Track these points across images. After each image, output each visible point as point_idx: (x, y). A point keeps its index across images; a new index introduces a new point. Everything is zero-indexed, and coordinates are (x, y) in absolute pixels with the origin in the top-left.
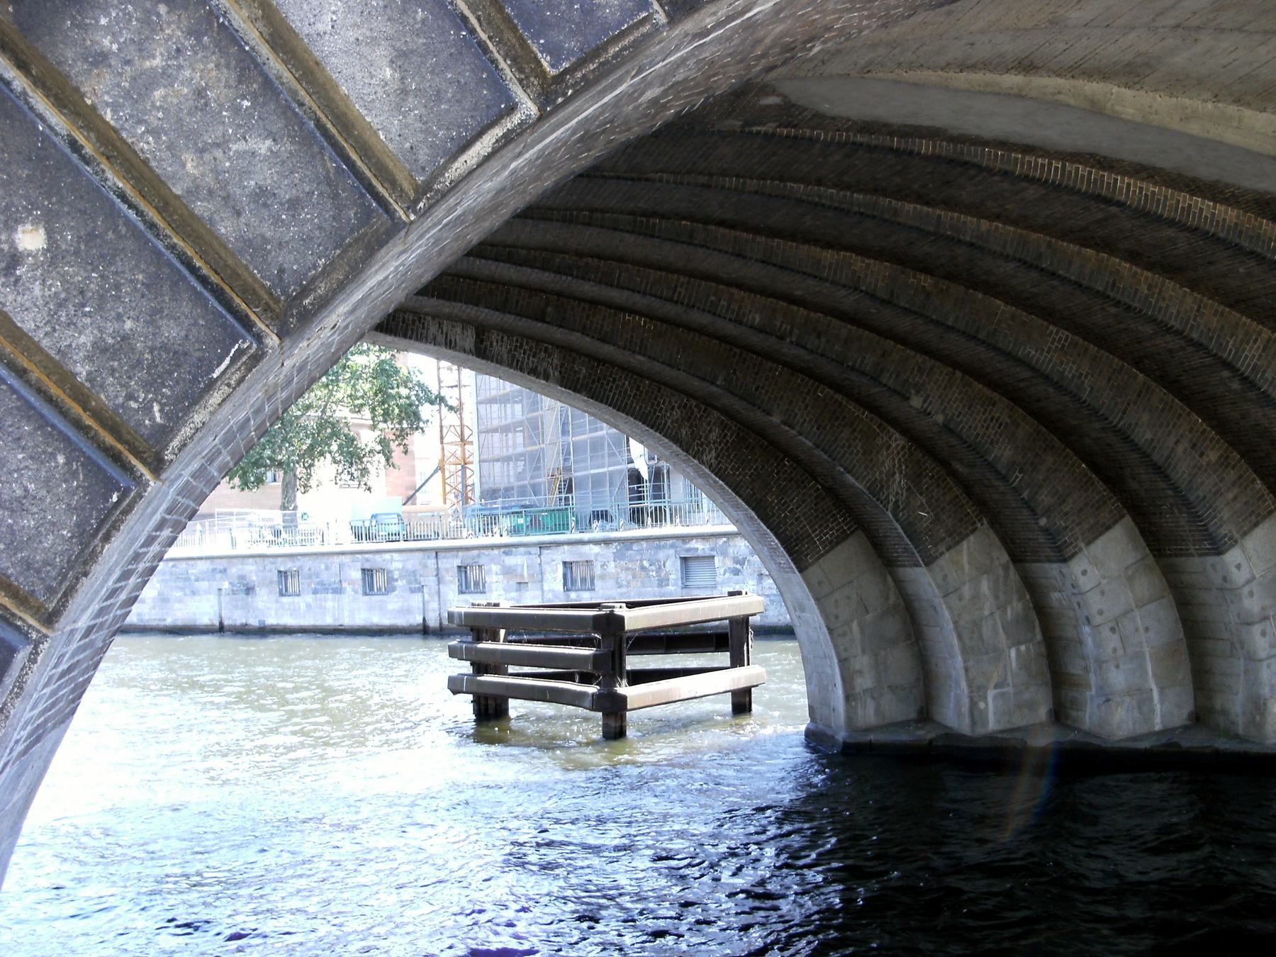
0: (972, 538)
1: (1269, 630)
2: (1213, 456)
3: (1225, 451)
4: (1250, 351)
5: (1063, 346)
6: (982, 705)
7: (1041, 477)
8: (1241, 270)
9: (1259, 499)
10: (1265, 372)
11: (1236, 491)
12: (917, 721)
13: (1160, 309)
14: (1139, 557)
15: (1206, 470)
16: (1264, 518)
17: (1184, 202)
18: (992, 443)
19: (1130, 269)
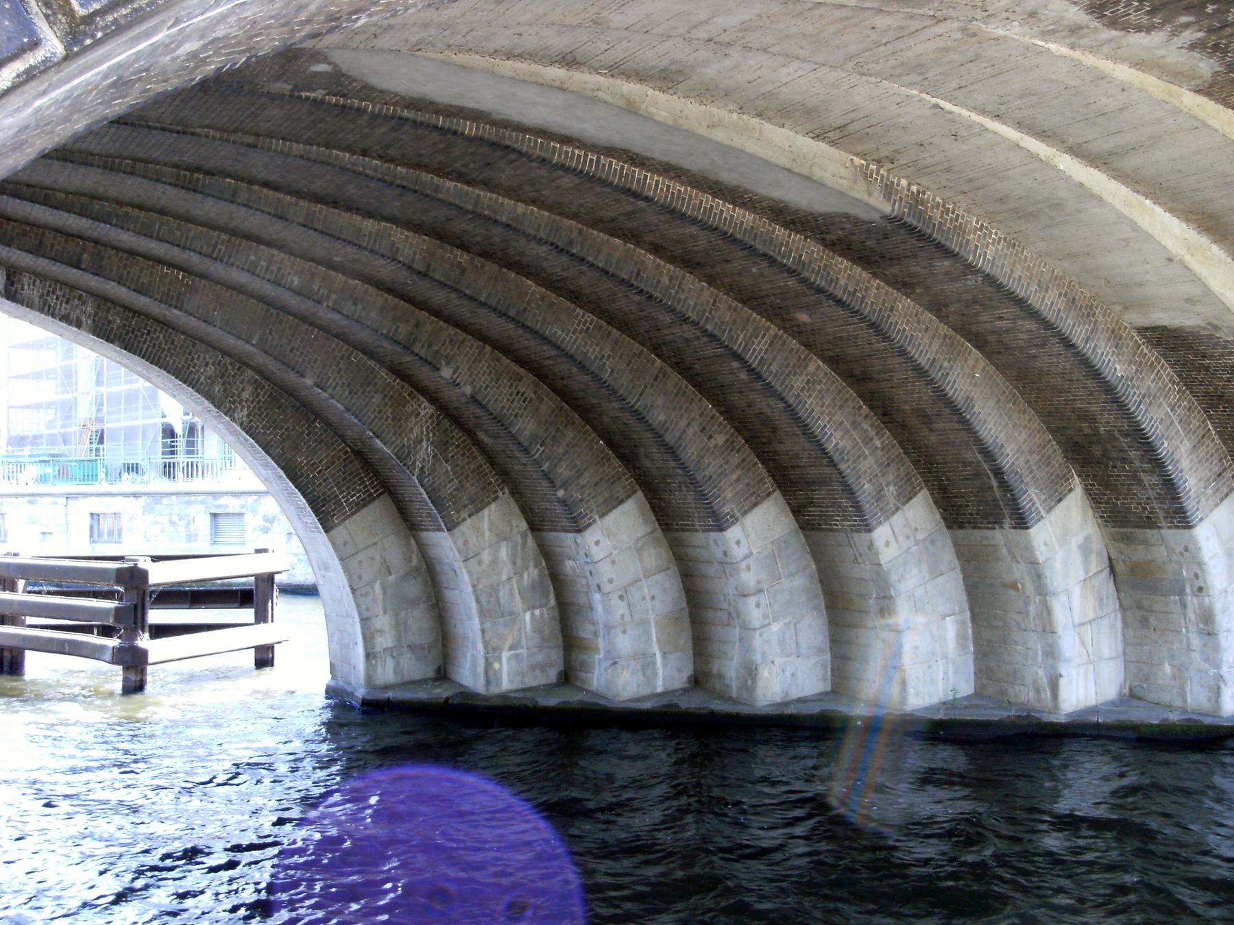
0: (493, 506)
1: (762, 602)
2: (720, 439)
6: (496, 666)
7: (561, 451)
8: (754, 270)
10: (770, 365)
13: (680, 300)
14: (649, 530)
16: (763, 499)
19: (654, 261)
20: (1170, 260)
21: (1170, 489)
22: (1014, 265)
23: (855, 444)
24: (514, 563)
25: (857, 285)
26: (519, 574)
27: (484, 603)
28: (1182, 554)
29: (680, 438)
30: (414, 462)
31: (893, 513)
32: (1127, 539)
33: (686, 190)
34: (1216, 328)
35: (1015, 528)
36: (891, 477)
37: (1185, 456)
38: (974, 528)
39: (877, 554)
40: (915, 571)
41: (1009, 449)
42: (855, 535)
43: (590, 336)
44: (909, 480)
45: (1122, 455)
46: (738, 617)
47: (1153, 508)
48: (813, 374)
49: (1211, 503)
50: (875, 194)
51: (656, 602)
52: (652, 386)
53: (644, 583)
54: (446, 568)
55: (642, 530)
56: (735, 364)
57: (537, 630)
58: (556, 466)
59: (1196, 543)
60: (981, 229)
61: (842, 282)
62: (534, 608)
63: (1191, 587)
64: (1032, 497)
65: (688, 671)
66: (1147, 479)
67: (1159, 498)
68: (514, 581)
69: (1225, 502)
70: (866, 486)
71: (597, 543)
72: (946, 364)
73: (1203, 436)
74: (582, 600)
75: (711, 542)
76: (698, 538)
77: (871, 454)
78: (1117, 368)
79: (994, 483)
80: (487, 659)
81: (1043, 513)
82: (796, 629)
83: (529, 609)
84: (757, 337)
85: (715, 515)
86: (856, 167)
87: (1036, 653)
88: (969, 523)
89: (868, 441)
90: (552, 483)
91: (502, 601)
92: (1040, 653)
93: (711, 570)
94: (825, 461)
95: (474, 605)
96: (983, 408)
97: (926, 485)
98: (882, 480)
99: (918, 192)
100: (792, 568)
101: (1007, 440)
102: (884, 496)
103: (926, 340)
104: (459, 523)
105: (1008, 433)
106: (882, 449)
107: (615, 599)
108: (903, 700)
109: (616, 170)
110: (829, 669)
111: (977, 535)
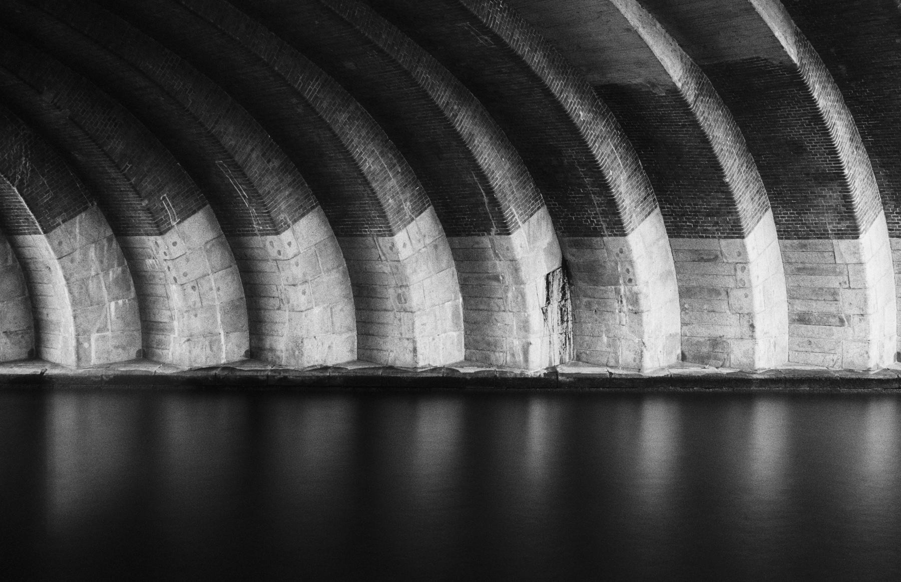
0: (83, 214)
1: (307, 291)
6: (86, 345)
8: (317, 22)
9: (306, 198)
10: (321, 102)
16: (308, 212)
24: (101, 262)
26: (106, 271)
27: (76, 295)
29: (246, 160)
30: (15, 173)
31: (409, 223)
32: (577, 245)
34: (654, 85)
35: (499, 234)
37: (623, 182)
38: (468, 235)
40: (424, 267)
41: (498, 174)
42: (380, 239)
51: (220, 293)
53: (212, 277)
54: (40, 265)
55: (210, 235)
56: (294, 101)
57: (121, 317)
58: (141, 180)
59: (628, 247)
62: (117, 299)
63: (624, 278)
64: (513, 211)
65: (245, 347)
68: (101, 276)
69: (648, 218)
70: (390, 201)
71: (175, 244)
72: (455, 107)
74: (160, 290)
75: (268, 243)
79: (486, 200)
80: (78, 341)
81: (520, 223)
82: (331, 312)
83: (113, 299)
85: (273, 222)
88: (464, 231)
89: (392, 167)
90: (138, 193)
91: (91, 293)
92: (515, 328)
93: (268, 267)
95: (67, 294)
98: (401, 197)
100: (329, 266)
102: (403, 209)
104: (54, 228)
107: (189, 290)
110: (356, 344)
111: (468, 241)
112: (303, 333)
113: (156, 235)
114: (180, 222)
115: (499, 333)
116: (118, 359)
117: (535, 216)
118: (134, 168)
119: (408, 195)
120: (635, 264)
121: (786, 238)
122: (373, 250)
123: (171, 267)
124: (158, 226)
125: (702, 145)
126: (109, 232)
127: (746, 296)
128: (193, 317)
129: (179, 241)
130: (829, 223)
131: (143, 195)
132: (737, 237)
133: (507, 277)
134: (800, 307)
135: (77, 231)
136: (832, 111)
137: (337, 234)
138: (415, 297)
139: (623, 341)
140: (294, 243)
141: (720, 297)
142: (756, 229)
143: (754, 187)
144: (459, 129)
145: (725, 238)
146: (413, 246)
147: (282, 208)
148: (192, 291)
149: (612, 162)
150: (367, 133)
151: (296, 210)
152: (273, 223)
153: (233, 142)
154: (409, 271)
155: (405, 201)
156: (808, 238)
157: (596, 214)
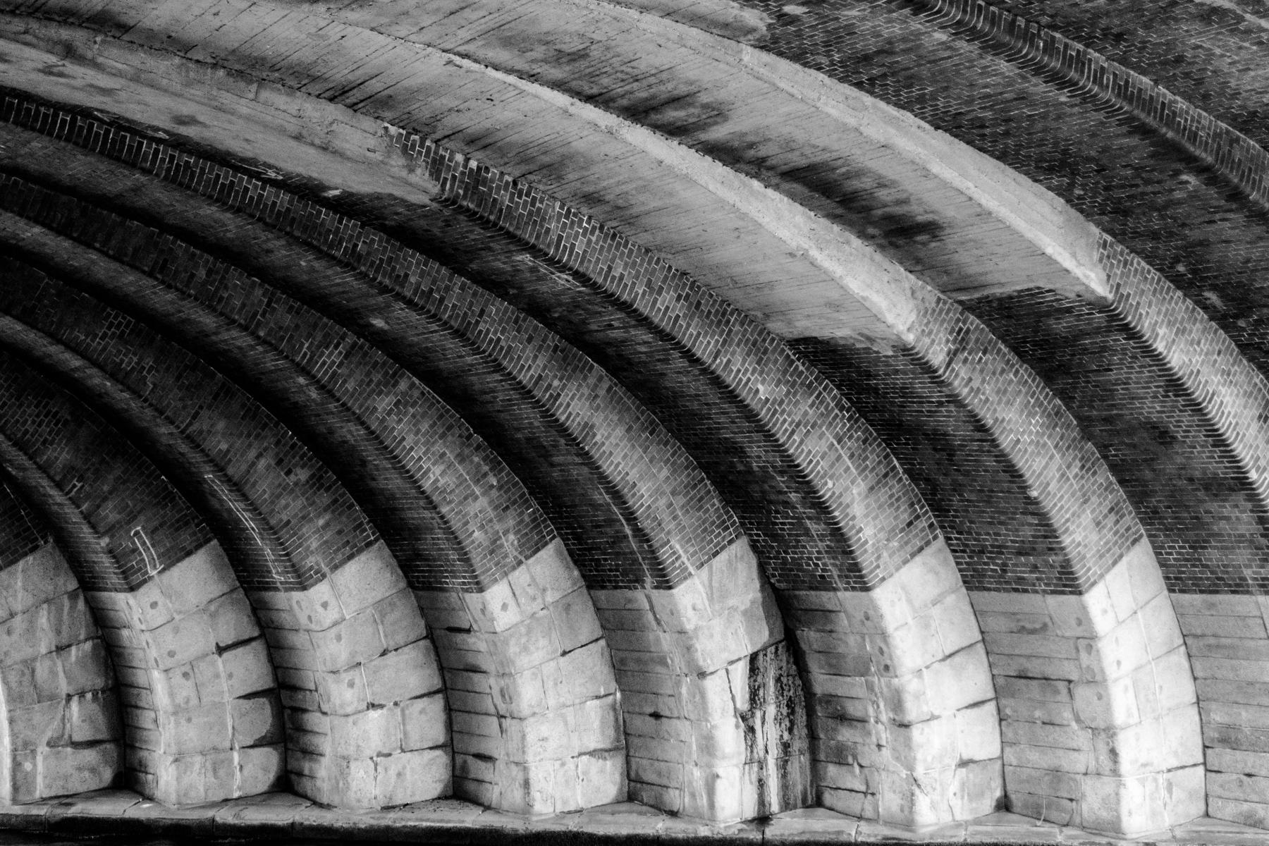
0: (30, 558)
1: (357, 681)
2: (303, 475)
3: (320, 469)
4: (329, 357)
5: (123, 333)
6: (28, 766)
7: (106, 488)
8: (303, 263)
9: (355, 529)
10: (345, 382)
11: (327, 516)
12: (443, 797)
13: (221, 299)
14: (226, 589)
15: (292, 491)
16: (360, 551)
17: (226, 178)
18: (44, 442)
19: (186, 251)
20: (792, 255)
21: (839, 540)
22: (613, 261)
23: (461, 480)
25: (434, 282)
27: (14, 685)
28: (863, 622)
31: (514, 568)
33: (196, 163)
34: (869, 339)
35: (656, 588)
36: (511, 523)
37: (857, 499)
38: (616, 588)
39: (492, 620)
40: (542, 642)
41: (644, 489)
42: (467, 596)
43: (126, 343)
44: (535, 527)
45: (781, 497)
46: (329, 701)
47: (824, 564)
48: (404, 394)
49: (897, 559)
50: (419, 171)
52: (209, 407)
56: (301, 380)
58: (98, 507)
59: (876, 608)
60: (567, 217)
61: (413, 279)
64: (676, 548)
66: (814, 527)
67: (830, 551)
69: (918, 559)
70: (476, 534)
72: (556, 383)
73: (886, 475)
76: (280, 599)
77: (484, 494)
78: (761, 389)
79: (628, 531)
80: (14, 759)
81: (691, 569)
84: (327, 348)
85: (296, 570)
86: (391, 137)
87: (690, 747)
89: (479, 478)
90: (93, 527)
93: (298, 640)
94: (422, 503)
96: (607, 438)
97: (560, 535)
98: (497, 527)
99: (479, 168)
101: (641, 478)
102: (502, 546)
103: (529, 352)
105: (636, 469)
106: (500, 488)
107: (177, 678)
108: (527, 809)
109: (97, 134)
112: (351, 751)
113: (125, 591)
114: (164, 570)
115: (672, 755)
116: (81, 788)
117: (723, 556)
118: (87, 488)
119: (511, 523)
120: (890, 640)
121: (1182, 591)
122: (461, 613)
123: (150, 641)
124: (125, 578)
125: (978, 435)
126: (72, 585)
127: (1100, 698)
128: (183, 721)
129: (161, 600)
130: (1246, 566)
131: (102, 530)
132: (1071, 593)
133: (677, 660)
134: (1218, 716)
135: (20, 584)
136: (1204, 370)
137: (411, 585)
138: (528, 693)
139: (884, 774)
140: (333, 603)
141: (1059, 698)
142: (1108, 577)
143: (1100, 503)
144: (563, 418)
145: (1053, 592)
146: (520, 603)
147: (312, 544)
148: (183, 681)
149: (832, 466)
150: (431, 426)
151: (339, 549)
152: (296, 571)
153: (224, 446)
154: (513, 649)
155: (506, 532)
156: (1217, 592)
157: (818, 552)
